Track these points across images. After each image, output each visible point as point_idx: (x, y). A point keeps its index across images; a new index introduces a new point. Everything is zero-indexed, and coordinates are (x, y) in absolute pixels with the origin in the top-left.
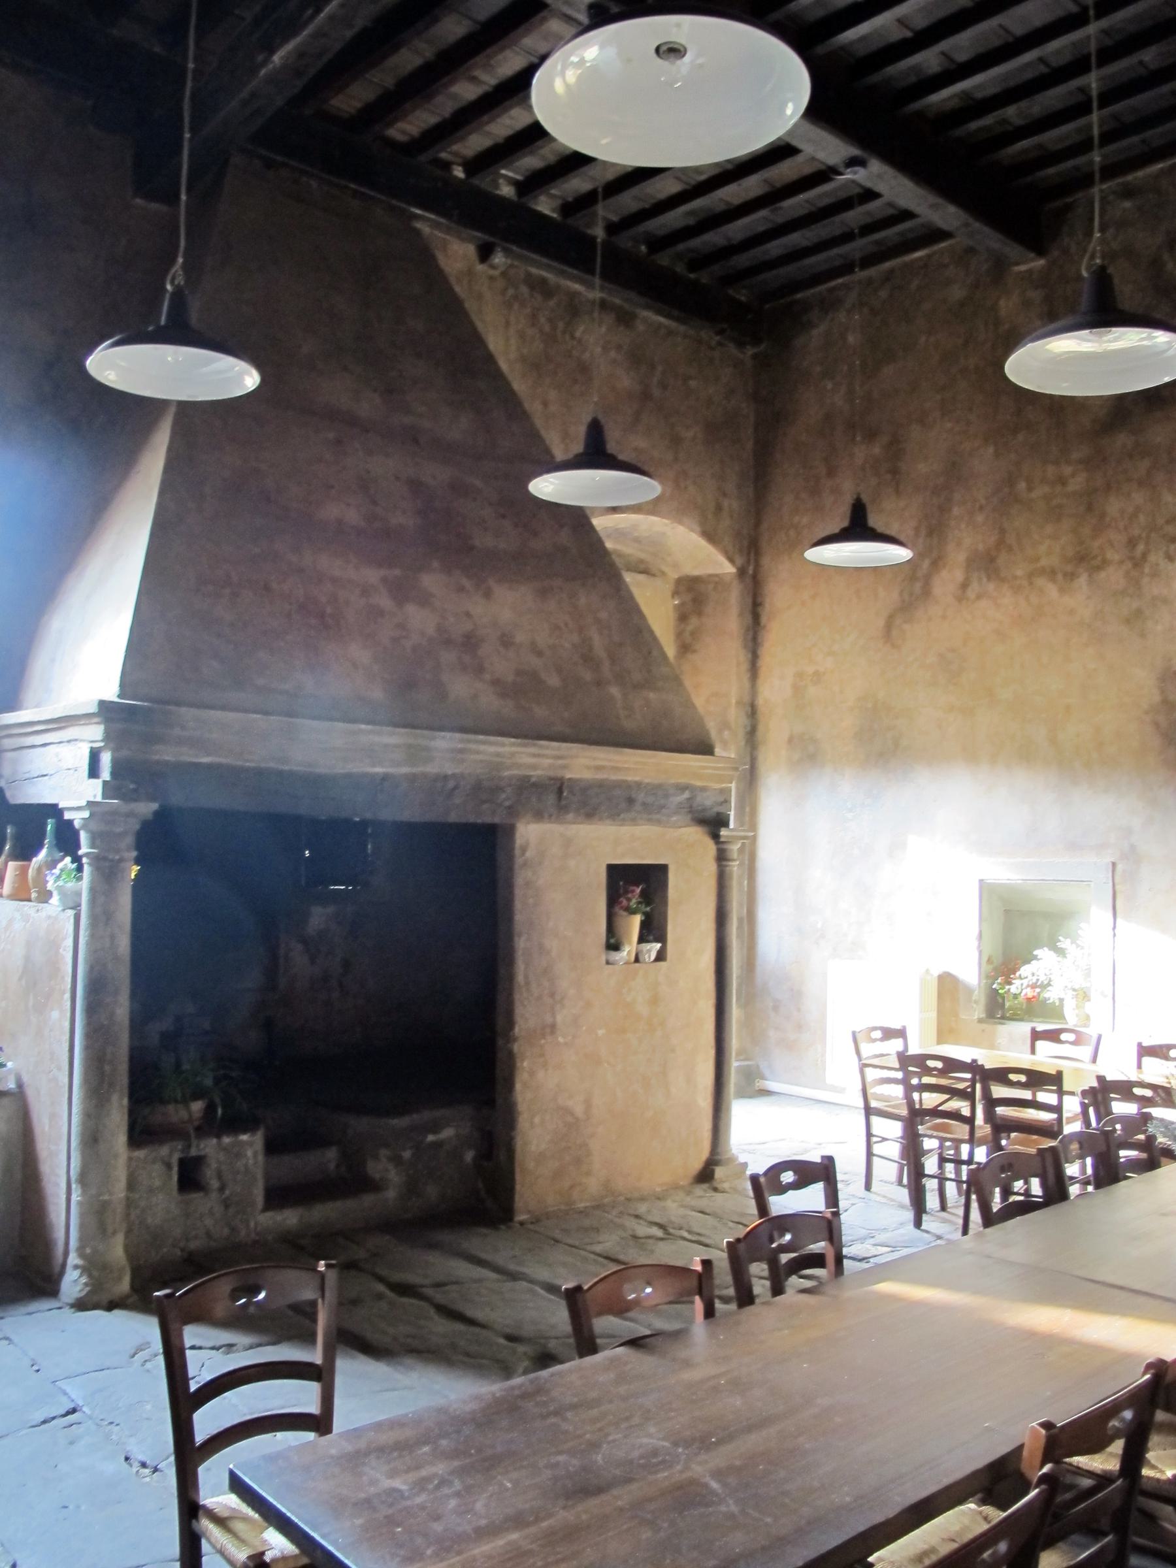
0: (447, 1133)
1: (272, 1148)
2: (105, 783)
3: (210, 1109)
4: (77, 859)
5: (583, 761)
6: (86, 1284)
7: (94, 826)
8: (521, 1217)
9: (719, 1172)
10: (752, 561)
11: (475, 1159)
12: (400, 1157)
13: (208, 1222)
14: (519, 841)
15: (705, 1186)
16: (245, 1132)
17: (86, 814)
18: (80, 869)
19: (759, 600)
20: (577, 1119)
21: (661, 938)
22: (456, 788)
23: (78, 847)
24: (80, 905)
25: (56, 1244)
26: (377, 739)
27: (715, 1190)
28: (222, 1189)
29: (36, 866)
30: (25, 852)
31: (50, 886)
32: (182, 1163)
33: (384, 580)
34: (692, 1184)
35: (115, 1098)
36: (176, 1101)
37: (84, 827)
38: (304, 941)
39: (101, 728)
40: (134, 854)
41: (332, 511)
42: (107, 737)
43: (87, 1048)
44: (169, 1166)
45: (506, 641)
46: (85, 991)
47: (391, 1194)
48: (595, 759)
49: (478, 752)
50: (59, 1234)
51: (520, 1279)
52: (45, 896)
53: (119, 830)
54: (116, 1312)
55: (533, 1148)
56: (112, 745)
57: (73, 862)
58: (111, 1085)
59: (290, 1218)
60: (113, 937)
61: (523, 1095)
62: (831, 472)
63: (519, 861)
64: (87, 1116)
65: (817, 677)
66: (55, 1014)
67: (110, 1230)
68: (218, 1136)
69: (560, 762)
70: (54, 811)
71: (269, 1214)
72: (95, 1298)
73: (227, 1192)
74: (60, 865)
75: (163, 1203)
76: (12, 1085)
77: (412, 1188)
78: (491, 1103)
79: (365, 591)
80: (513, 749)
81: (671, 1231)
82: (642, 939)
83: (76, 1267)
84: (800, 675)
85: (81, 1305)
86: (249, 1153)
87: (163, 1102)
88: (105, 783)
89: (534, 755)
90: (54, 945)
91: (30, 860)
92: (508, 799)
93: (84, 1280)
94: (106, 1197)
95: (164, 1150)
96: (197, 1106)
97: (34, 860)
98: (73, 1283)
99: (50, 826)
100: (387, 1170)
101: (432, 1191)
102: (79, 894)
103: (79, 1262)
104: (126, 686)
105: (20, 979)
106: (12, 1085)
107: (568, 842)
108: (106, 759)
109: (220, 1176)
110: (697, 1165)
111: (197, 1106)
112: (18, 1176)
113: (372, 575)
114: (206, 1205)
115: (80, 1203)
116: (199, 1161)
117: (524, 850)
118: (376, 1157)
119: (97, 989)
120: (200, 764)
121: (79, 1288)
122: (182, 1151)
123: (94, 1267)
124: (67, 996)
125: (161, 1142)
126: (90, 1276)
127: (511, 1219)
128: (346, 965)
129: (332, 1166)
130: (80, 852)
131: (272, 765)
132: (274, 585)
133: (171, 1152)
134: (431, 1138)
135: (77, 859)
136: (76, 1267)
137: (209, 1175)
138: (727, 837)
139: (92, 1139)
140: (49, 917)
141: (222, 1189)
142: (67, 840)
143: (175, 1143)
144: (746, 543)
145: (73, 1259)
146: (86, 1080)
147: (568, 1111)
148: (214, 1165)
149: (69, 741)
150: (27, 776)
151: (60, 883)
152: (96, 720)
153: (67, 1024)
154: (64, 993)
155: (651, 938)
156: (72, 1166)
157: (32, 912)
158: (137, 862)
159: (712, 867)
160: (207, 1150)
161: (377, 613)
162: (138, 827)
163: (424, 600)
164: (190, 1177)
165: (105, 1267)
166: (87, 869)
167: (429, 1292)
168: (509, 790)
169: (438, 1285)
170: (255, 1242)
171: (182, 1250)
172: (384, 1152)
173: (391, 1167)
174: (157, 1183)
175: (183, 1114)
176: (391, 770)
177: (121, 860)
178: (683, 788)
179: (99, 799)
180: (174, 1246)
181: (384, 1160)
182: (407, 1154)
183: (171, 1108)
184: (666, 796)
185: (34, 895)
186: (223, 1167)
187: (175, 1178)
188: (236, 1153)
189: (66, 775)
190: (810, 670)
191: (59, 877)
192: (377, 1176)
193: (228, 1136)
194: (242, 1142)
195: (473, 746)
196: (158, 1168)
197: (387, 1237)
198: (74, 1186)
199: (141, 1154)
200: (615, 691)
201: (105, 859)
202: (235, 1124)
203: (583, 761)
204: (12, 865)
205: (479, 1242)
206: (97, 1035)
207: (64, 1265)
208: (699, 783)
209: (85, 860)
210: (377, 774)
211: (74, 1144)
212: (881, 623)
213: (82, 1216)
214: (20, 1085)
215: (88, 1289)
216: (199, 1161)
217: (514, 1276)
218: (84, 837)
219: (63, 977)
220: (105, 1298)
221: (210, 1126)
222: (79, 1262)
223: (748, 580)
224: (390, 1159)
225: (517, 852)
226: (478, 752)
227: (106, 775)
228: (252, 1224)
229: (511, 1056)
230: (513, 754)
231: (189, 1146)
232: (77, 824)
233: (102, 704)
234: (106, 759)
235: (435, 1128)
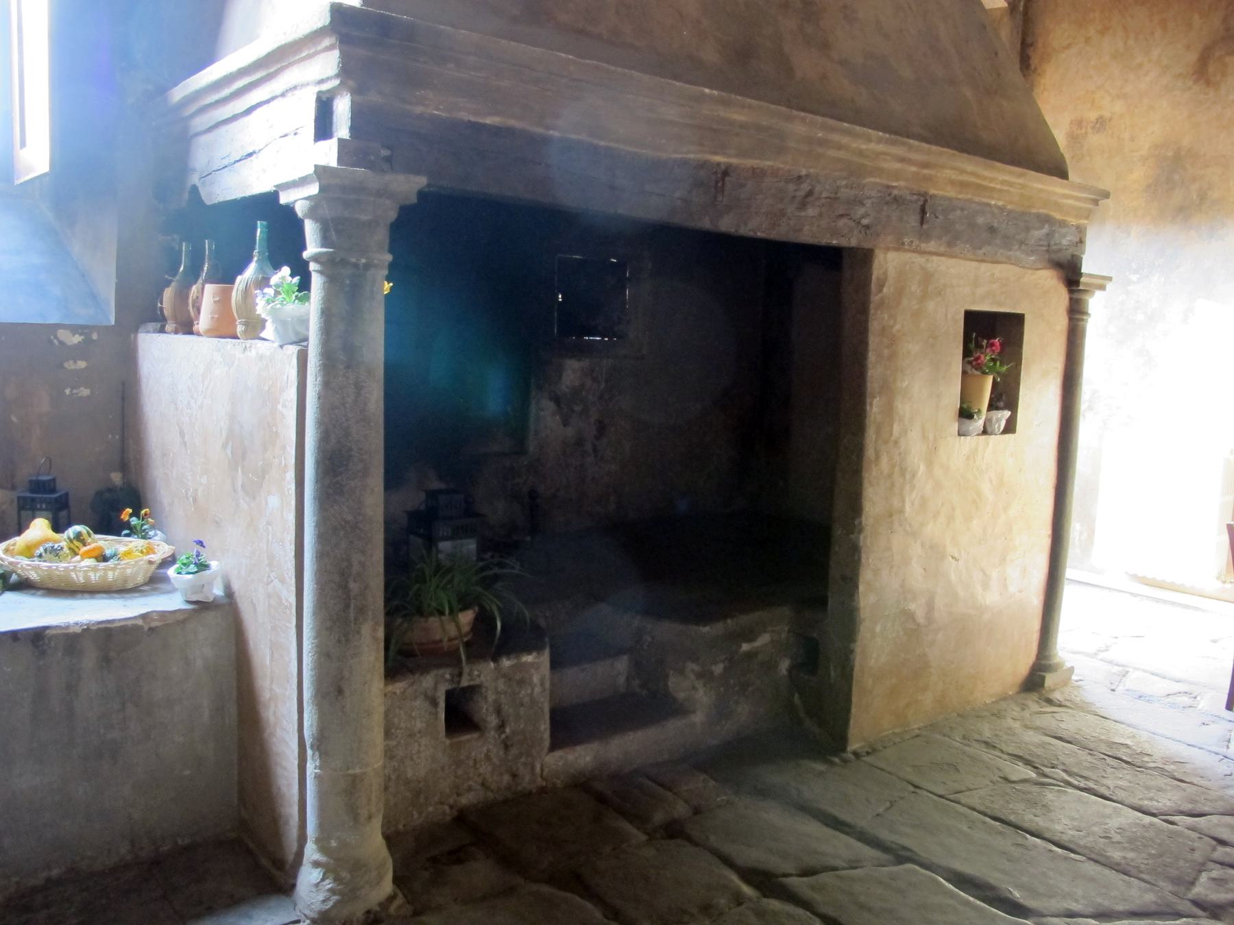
0: (764, 639)
2: (341, 142)
5: (949, 173)
6: (332, 891)
7: (326, 212)
8: (854, 745)
9: (1050, 680)
11: (790, 671)
13: (485, 769)
14: (876, 273)
15: (1035, 696)
16: (529, 652)
17: (314, 189)
18: (305, 286)
19: (1029, 40)
21: (1012, 405)
22: (810, 193)
24: (306, 339)
25: (287, 823)
26: (723, 112)
27: (1050, 702)
28: (501, 727)
29: (242, 286)
31: (261, 308)
32: (449, 694)
34: (1019, 693)
35: (366, 629)
36: (441, 613)
37: (313, 213)
38: (557, 400)
39: (336, 54)
40: (389, 258)
42: (346, 71)
43: (321, 556)
44: (434, 703)
47: (698, 718)
49: (839, 147)
52: (254, 327)
53: (364, 217)
55: (872, 663)
56: (351, 83)
58: (361, 610)
60: (358, 387)
63: (875, 298)
64: (324, 655)
65: (1101, 124)
66: (274, 501)
67: (364, 813)
69: (926, 171)
75: (429, 750)
76: (218, 591)
78: (820, 603)
80: (881, 147)
81: (1047, 770)
82: (992, 406)
83: (316, 864)
86: (536, 679)
87: (420, 612)
88: (341, 142)
89: (902, 160)
92: (866, 215)
93: (328, 884)
94: (358, 771)
95: (427, 681)
97: (239, 278)
100: (694, 688)
102: (304, 321)
103: (317, 856)
105: (224, 446)
106: (218, 591)
107: (927, 277)
109: (498, 711)
112: (232, 710)
115: (317, 777)
117: (881, 286)
119: (335, 465)
120: (484, 125)
121: (321, 897)
122: (452, 681)
124: (291, 475)
125: (425, 670)
126: (337, 879)
127: (844, 749)
129: (622, 680)
130: (306, 255)
133: (436, 683)
134: (745, 647)
137: (484, 710)
138: (1086, 284)
139: (333, 688)
140: (261, 357)
141: (501, 727)
143: (441, 671)
145: (311, 852)
147: (910, 616)
148: (491, 697)
150: (226, 162)
153: (291, 517)
155: (1001, 404)
156: (306, 724)
158: (389, 279)
159: (1062, 322)
160: (482, 678)
162: (393, 215)
164: (459, 716)
165: (357, 866)
166: (317, 281)
167: (795, 882)
168: (868, 203)
169: (807, 872)
171: (451, 807)
172: (692, 666)
173: (699, 684)
174: (419, 725)
177: (367, 267)
178: (1047, 220)
179: (333, 163)
180: (442, 803)
181: (692, 677)
182: (718, 669)
183: (434, 621)
184: (1028, 229)
185: (240, 329)
186: (503, 699)
187: (442, 716)
188: (518, 680)
190: (1093, 116)
192: (681, 696)
193: (509, 659)
194: (525, 663)
195: (835, 137)
198: (309, 752)
199: (399, 687)
203: (949, 173)
204: (210, 289)
205: (817, 782)
206: (336, 533)
209: (313, 266)
210: (718, 164)
212: (1193, 57)
213: (322, 796)
214: (229, 593)
215: (336, 898)
218: (311, 230)
219: (284, 448)
222: (317, 856)
223: (1019, 17)
224: (700, 676)
225: (873, 287)
226: (839, 147)
227: (342, 129)
230: (878, 155)
231: (460, 675)
232: (300, 209)
234: (343, 107)
235: (750, 635)
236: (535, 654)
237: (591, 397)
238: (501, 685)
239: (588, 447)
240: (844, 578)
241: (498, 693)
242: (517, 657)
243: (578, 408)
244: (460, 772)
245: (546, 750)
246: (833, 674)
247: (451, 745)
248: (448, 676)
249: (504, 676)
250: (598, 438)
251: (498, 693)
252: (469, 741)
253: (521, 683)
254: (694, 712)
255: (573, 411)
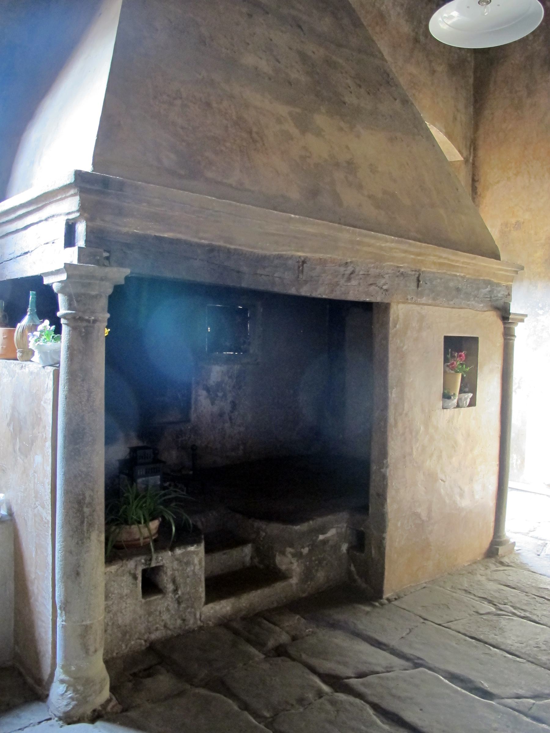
0: (332, 533)
1: (208, 551)
3: (164, 527)
4: (56, 322)
5: (432, 258)
9: (502, 550)
10: (472, 154)
11: (348, 550)
12: (301, 553)
15: (493, 560)
16: (192, 544)
17: (64, 277)
18: (58, 331)
20: (423, 521)
21: (474, 390)
23: (57, 309)
24: (59, 363)
28: (175, 591)
29: (21, 330)
30: (12, 318)
31: (31, 346)
32: (144, 572)
33: (290, 113)
34: (483, 559)
35: (94, 536)
37: (63, 290)
38: (208, 390)
39: (77, 199)
41: (249, 60)
42: (82, 208)
44: (135, 578)
45: (373, 169)
46: (65, 437)
48: (440, 257)
50: (46, 648)
51: (421, 665)
52: (28, 355)
54: (99, 724)
57: (51, 325)
58: (91, 525)
59: (224, 607)
61: (391, 507)
62: (530, 93)
64: (68, 552)
65: (518, 225)
66: (38, 459)
67: (92, 649)
68: (172, 549)
70: (36, 282)
71: (210, 605)
72: (81, 711)
73: (180, 592)
74: (40, 328)
75: (132, 605)
76: (4, 512)
77: (308, 575)
79: (279, 121)
83: (62, 682)
84: (506, 224)
85: (69, 719)
86: (196, 561)
88: (80, 248)
89: (405, 252)
90: (35, 398)
91: (15, 326)
93: (70, 694)
94: (88, 622)
95: (131, 564)
96: (154, 525)
98: (59, 695)
99: (32, 295)
100: (291, 563)
101: (321, 575)
103: (63, 677)
104: (98, 159)
105: (9, 425)
108: (81, 228)
109: (174, 581)
110: (486, 544)
111: (154, 525)
113: (283, 110)
114: (163, 604)
115: (63, 627)
116: (158, 570)
118: (283, 553)
121: (65, 703)
122: (145, 564)
123: (80, 683)
124: (49, 444)
125: (129, 557)
126: (76, 691)
128: (234, 405)
129: (248, 559)
130: (59, 314)
131: (221, 243)
132: (215, 105)
133: (135, 565)
134: (321, 537)
135: (56, 322)
136: (62, 682)
139: (74, 573)
140: (31, 373)
141: (175, 591)
142: (47, 307)
143: (138, 558)
144: (468, 144)
145: (59, 674)
146: (67, 521)
148: (169, 573)
149: (46, 220)
150: (12, 256)
151: (41, 343)
152: (72, 192)
154: (45, 441)
156: (57, 594)
157: (17, 369)
160: (164, 561)
161: (290, 137)
163: (319, 133)
164: (150, 584)
165: (88, 682)
166: (65, 329)
167: (354, 682)
169: (361, 675)
170: (201, 628)
171: (145, 641)
172: (289, 550)
173: (294, 560)
175: (145, 532)
176: (309, 255)
178: (488, 283)
179: (75, 262)
181: (290, 556)
182: (305, 551)
183: (134, 528)
184: (478, 289)
185: (19, 355)
187: (140, 585)
189: (45, 251)
190: (513, 221)
191: (39, 339)
192: (283, 567)
193: (180, 549)
195: (366, 240)
196: (127, 579)
197: (298, 617)
198: (59, 611)
199: (113, 568)
200: (442, 211)
201: (81, 319)
202: (185, 536)
205: (366, 618)
207: (52, 675)
208: (495, 281)
209: (63, 321)
211: (57, 577)
213: (66, 639)
214: (10, 513)
215: (74, 703)
216: (158, 570)
217: (417, 663)
218: (61, 299)
219: (45, 427)
220: (88, 710)
221: (165, 540)
223: (470, 166)
224: (294, 555)
225: (391, 324)
227: (81, 242)
228: (198, 616)
229: (384, 477)
230: (391, 249)
231: (151, 560)
233: (79, 174)
234: (81, 228)
235: (323, 530)
236: (195, 546)
237: (228, 388)
238: (175, 565)
239: (226, 417)
240: (378, 495)
241: (173, 570)
242: (185, 548)
243: (220, 394)
244: (151, 619)
245: (203, 604)
246: (373, 552)
247: (146, 603)
248: (143, 561)
249: (177, 559)
250: (232, 412)
251: (173, 570)
252: (155, 600)
253: (188, 563)
254: (291, 577)
255: (217, 396)
